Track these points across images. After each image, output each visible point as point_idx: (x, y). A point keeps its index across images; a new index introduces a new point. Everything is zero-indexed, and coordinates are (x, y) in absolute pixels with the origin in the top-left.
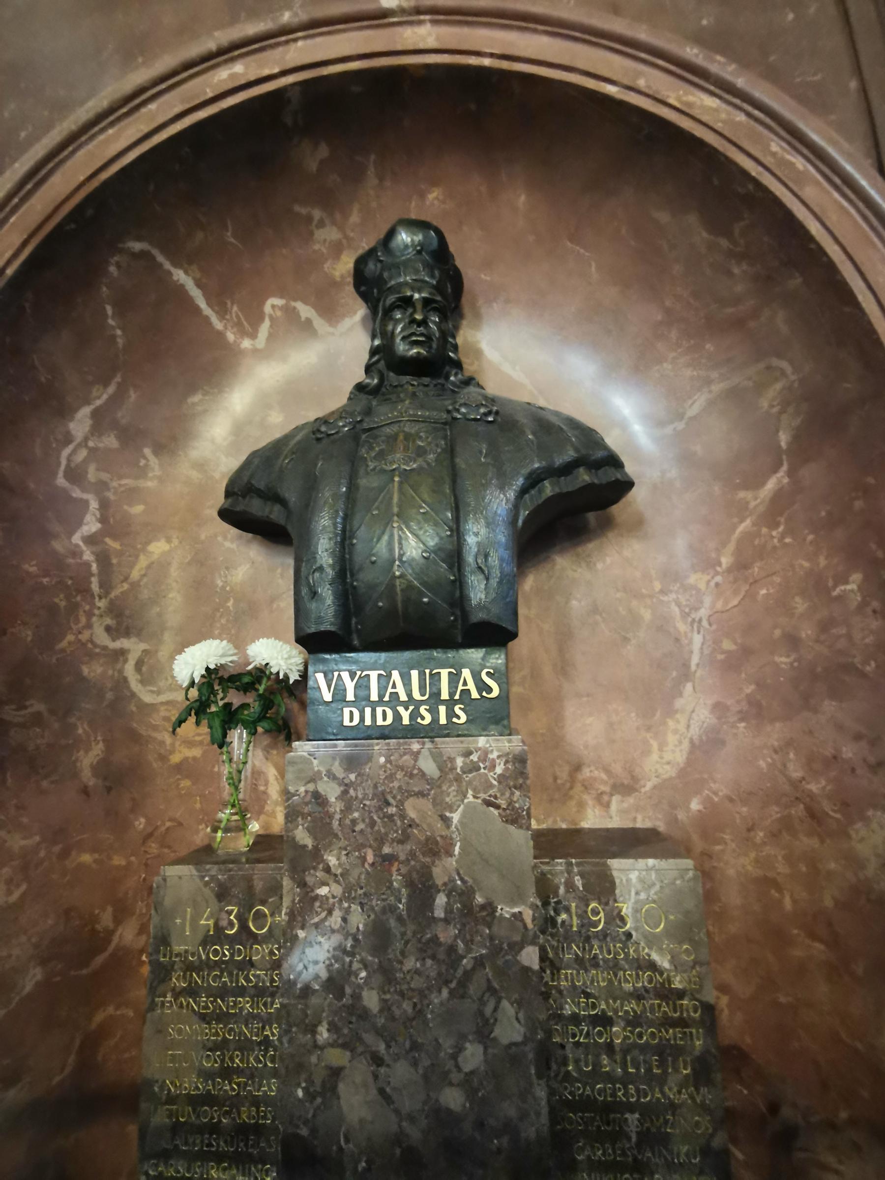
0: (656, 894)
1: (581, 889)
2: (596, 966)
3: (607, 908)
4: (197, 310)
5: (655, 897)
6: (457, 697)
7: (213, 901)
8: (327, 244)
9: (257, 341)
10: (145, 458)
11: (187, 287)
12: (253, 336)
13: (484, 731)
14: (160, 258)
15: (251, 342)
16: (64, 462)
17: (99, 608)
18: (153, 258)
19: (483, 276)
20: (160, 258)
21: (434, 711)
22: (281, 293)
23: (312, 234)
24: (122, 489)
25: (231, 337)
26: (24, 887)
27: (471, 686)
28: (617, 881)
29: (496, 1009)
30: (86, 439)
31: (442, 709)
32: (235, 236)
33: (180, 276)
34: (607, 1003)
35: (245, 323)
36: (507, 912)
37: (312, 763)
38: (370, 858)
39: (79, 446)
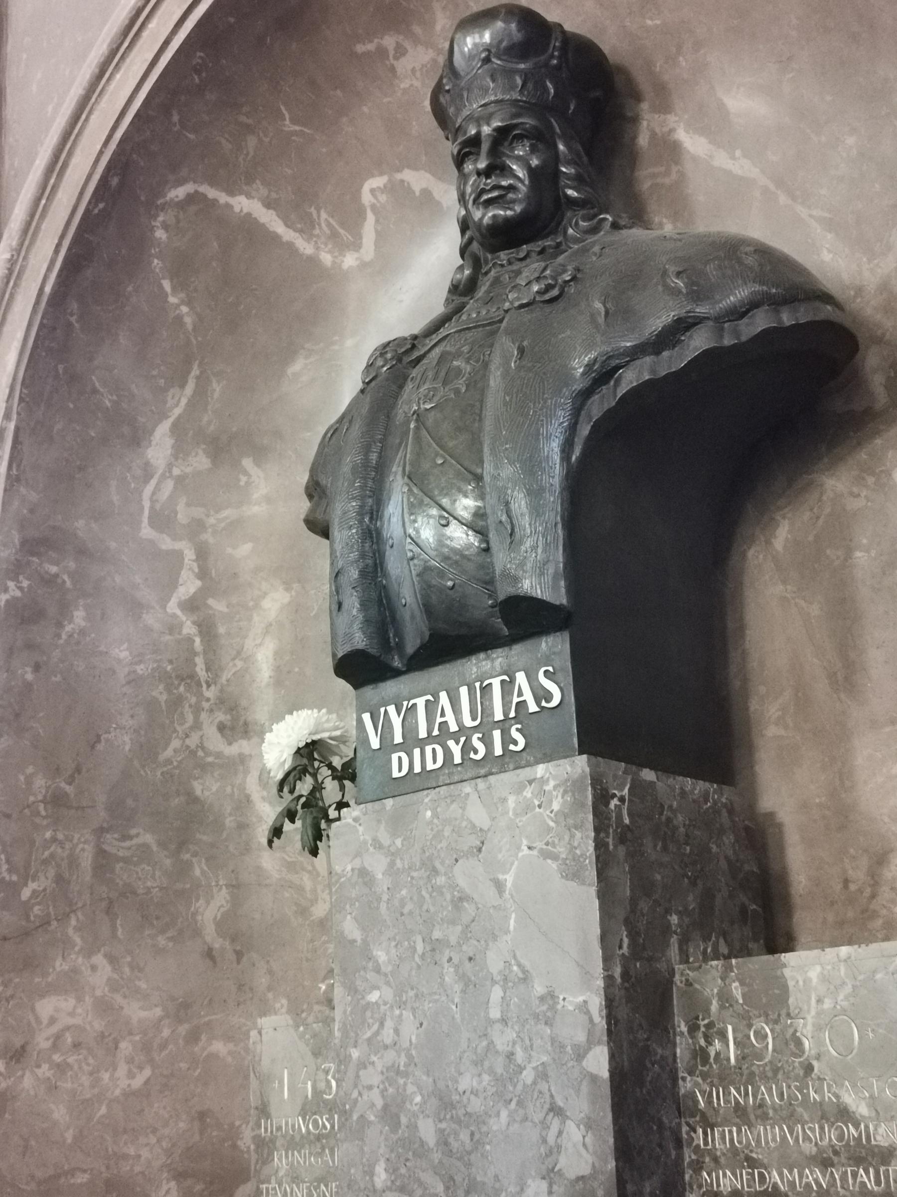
0: (846, 998)
1: (741, 1001)
2: (764, 1117)
3: (778, 1028)
4: (275, 238)
5: (845, 1004)
6: (512, 714)
7: (309, 1058)
8: (418, 74)
9: (362, 251)
10: (246, 473)
11: (255, 215)
12: (356, 246)
13: (547, 758)
14: (212, 193)
15: (356, 255)
16: (147, 504)
17: (208, 700)
18: (205, 196)
19: (649, 22)
20: (212, 193)
21: (487, 741)
22: (379, 166)
23: (393, 69)
24: (223, 525)
25: (326, 258)
26: (147, 1072)
27: (528, 696)
28: (791, 984)
29: (560, 1133)
30: (170, 466)
31: (497, 734)
32: (294, 121)
33: (244, 204)
34: (781, 1175)
35: (342, 231)
36: (571, 1002)
37: (357, 831)
38: (420, 947)
39: (163, 477)
